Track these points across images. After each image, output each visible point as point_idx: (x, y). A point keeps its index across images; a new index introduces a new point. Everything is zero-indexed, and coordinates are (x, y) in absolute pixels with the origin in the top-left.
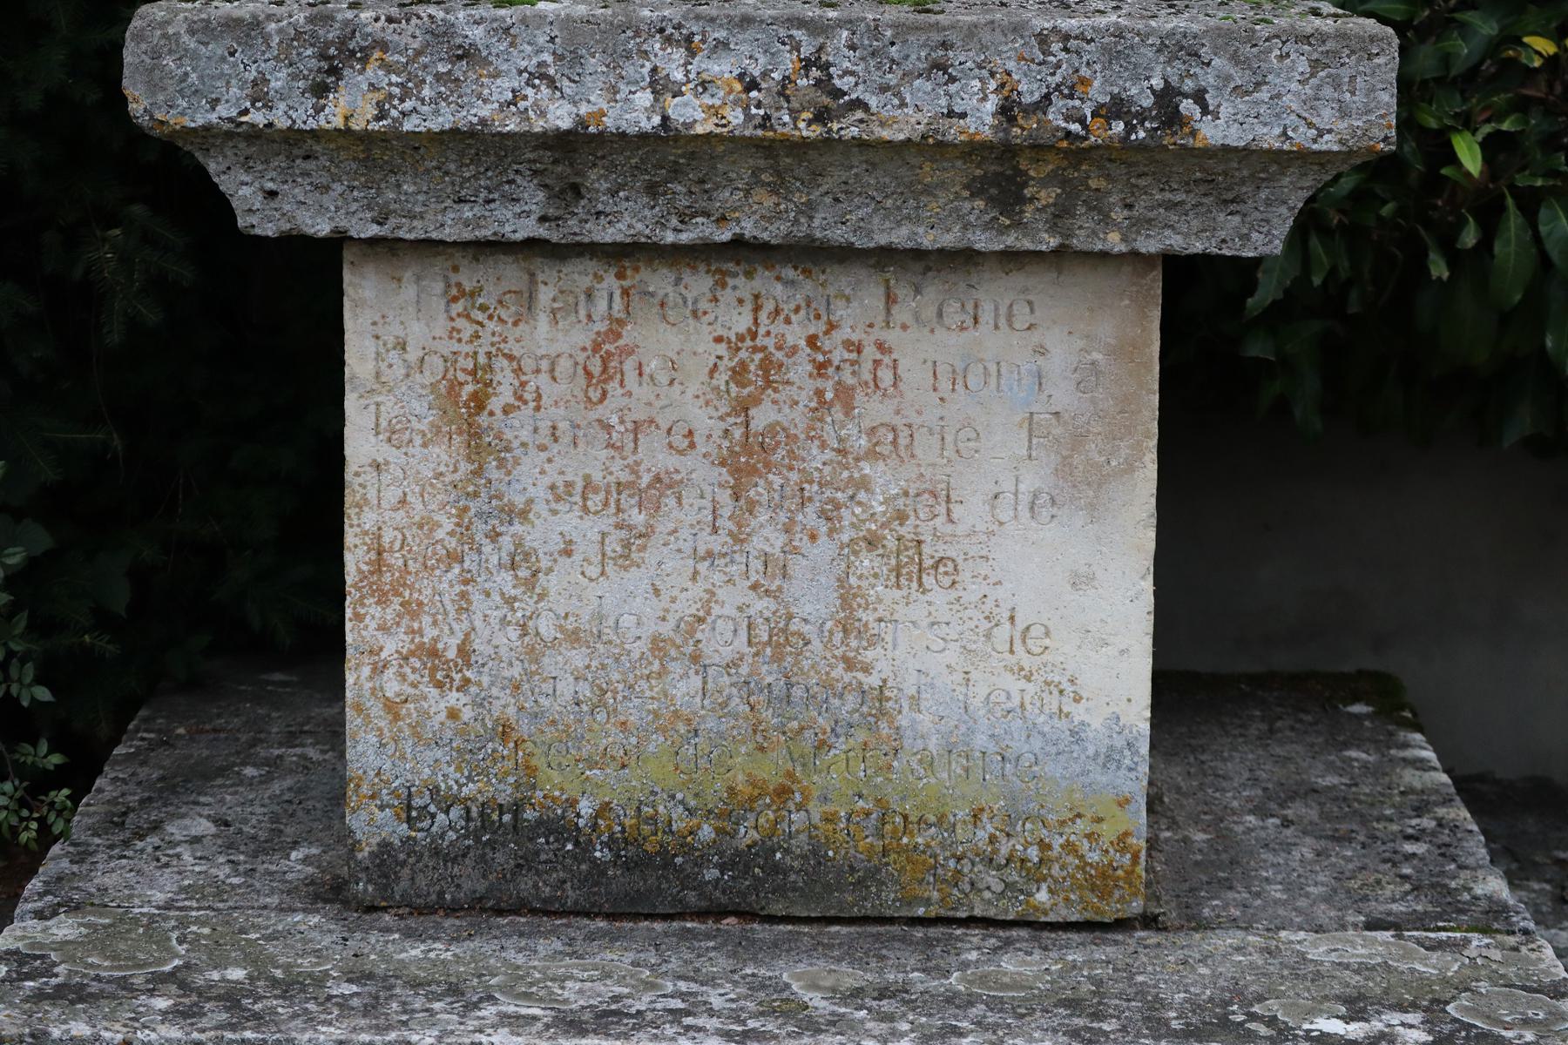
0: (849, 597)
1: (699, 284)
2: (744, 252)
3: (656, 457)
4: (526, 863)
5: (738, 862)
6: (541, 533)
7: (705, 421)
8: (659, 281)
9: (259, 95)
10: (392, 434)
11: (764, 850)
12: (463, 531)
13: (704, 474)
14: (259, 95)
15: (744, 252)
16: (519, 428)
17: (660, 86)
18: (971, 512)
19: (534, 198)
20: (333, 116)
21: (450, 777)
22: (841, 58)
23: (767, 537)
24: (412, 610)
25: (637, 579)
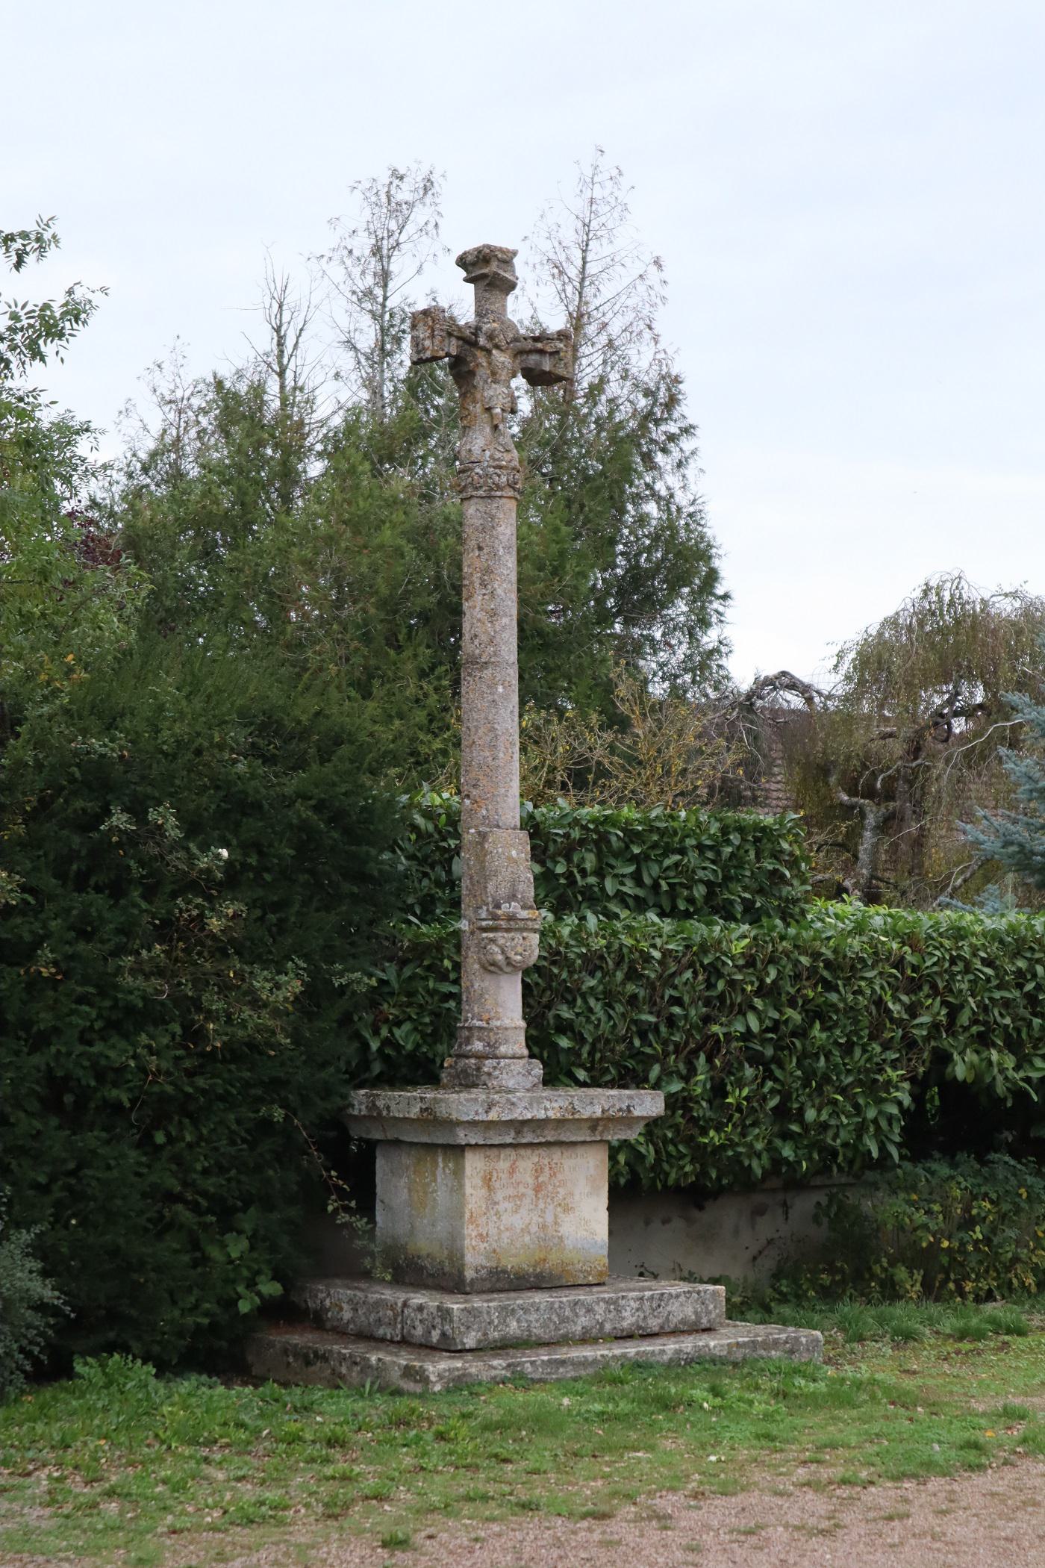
0: (556, 1216)
1: (529, 1151)
2: (548, 1144)
3: (522, 1189)
4: (498, 1280)
5: (536, 1276)
6: (500, 1208)
7: (530, 1181)
8: (522, 1152)
9: (477, 1113)
10: (474, 1187)
11: (541, 1273)
12: (487, 1208)
13: (530, 1192)
14: (477, 1113)
15: (548, 1144)
16: (497, 1185)
17: (546, 1109)
18: (577, 1198)
19: (513, 1134)
20: (490, 1118)
21: (484, 1262)
22: (576, 1102)
23: (541, 1205)
24: (477, 1226)
25: (518, 1216)
